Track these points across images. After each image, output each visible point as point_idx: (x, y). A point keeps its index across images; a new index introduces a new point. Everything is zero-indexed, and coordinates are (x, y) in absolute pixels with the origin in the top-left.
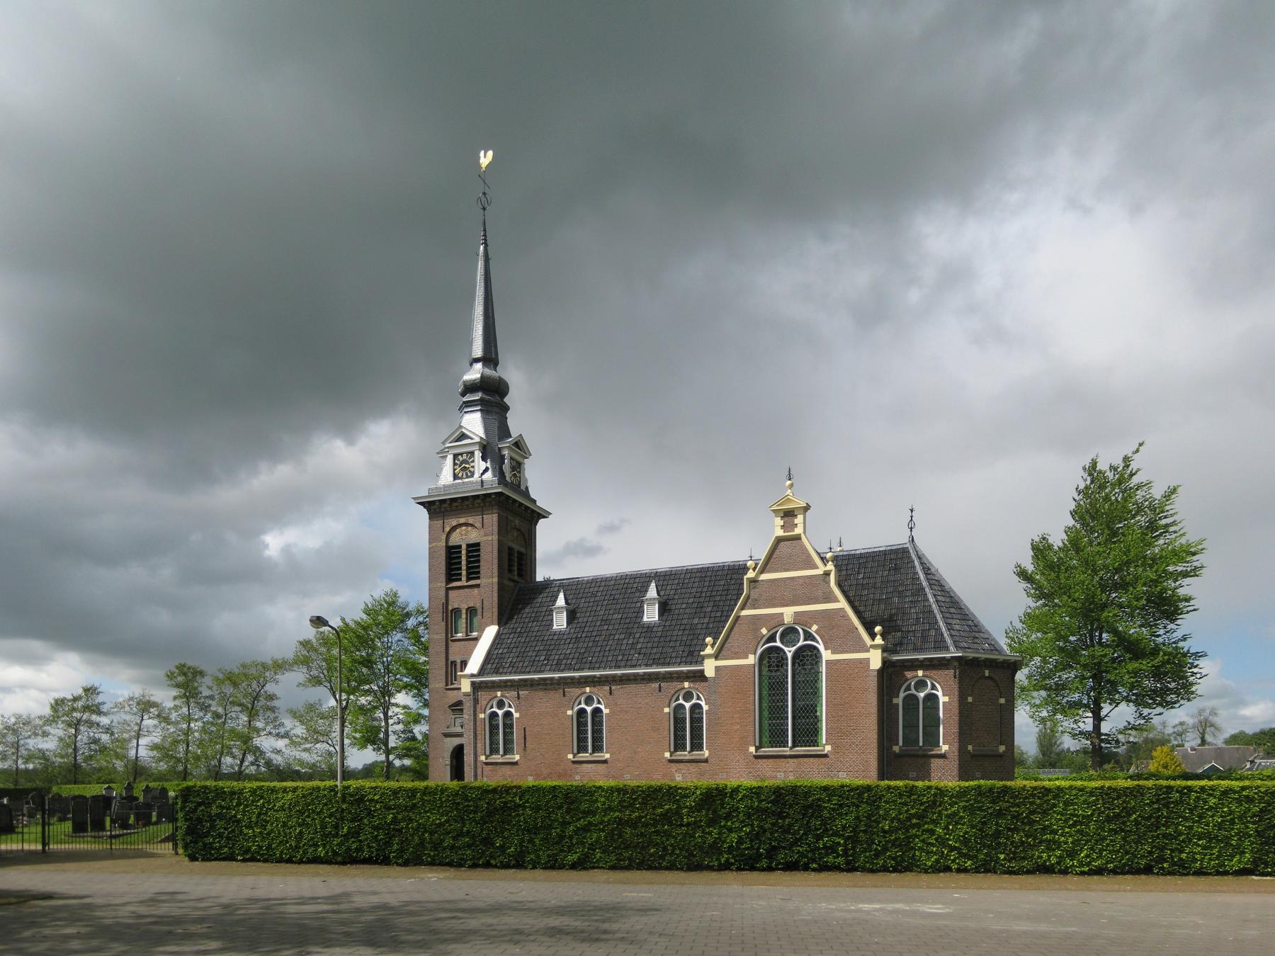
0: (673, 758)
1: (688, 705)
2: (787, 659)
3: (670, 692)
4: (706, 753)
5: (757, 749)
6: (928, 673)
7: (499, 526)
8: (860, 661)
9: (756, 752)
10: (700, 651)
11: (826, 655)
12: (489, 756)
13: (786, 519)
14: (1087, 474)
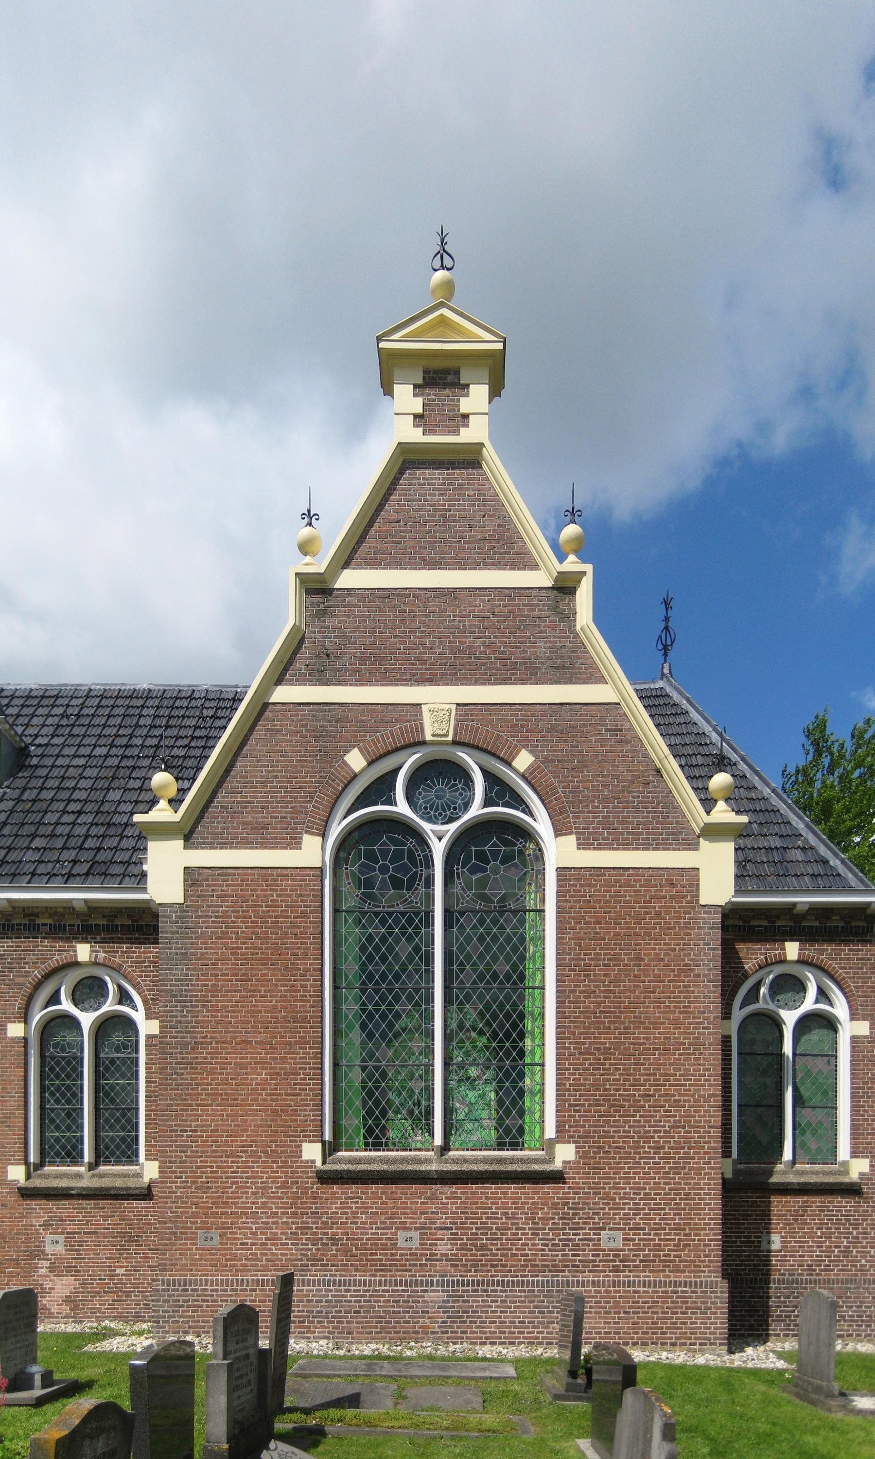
0: (37, 1183)
1: (87, 1019)
2: (429, 862)
3: (27, 975)
4: (150, 1170)
5: (330, 1149)
6: (813, 952)
8: (671, 876)
9: (324, 1163)
13: (432, 393)
14: (810, 742)
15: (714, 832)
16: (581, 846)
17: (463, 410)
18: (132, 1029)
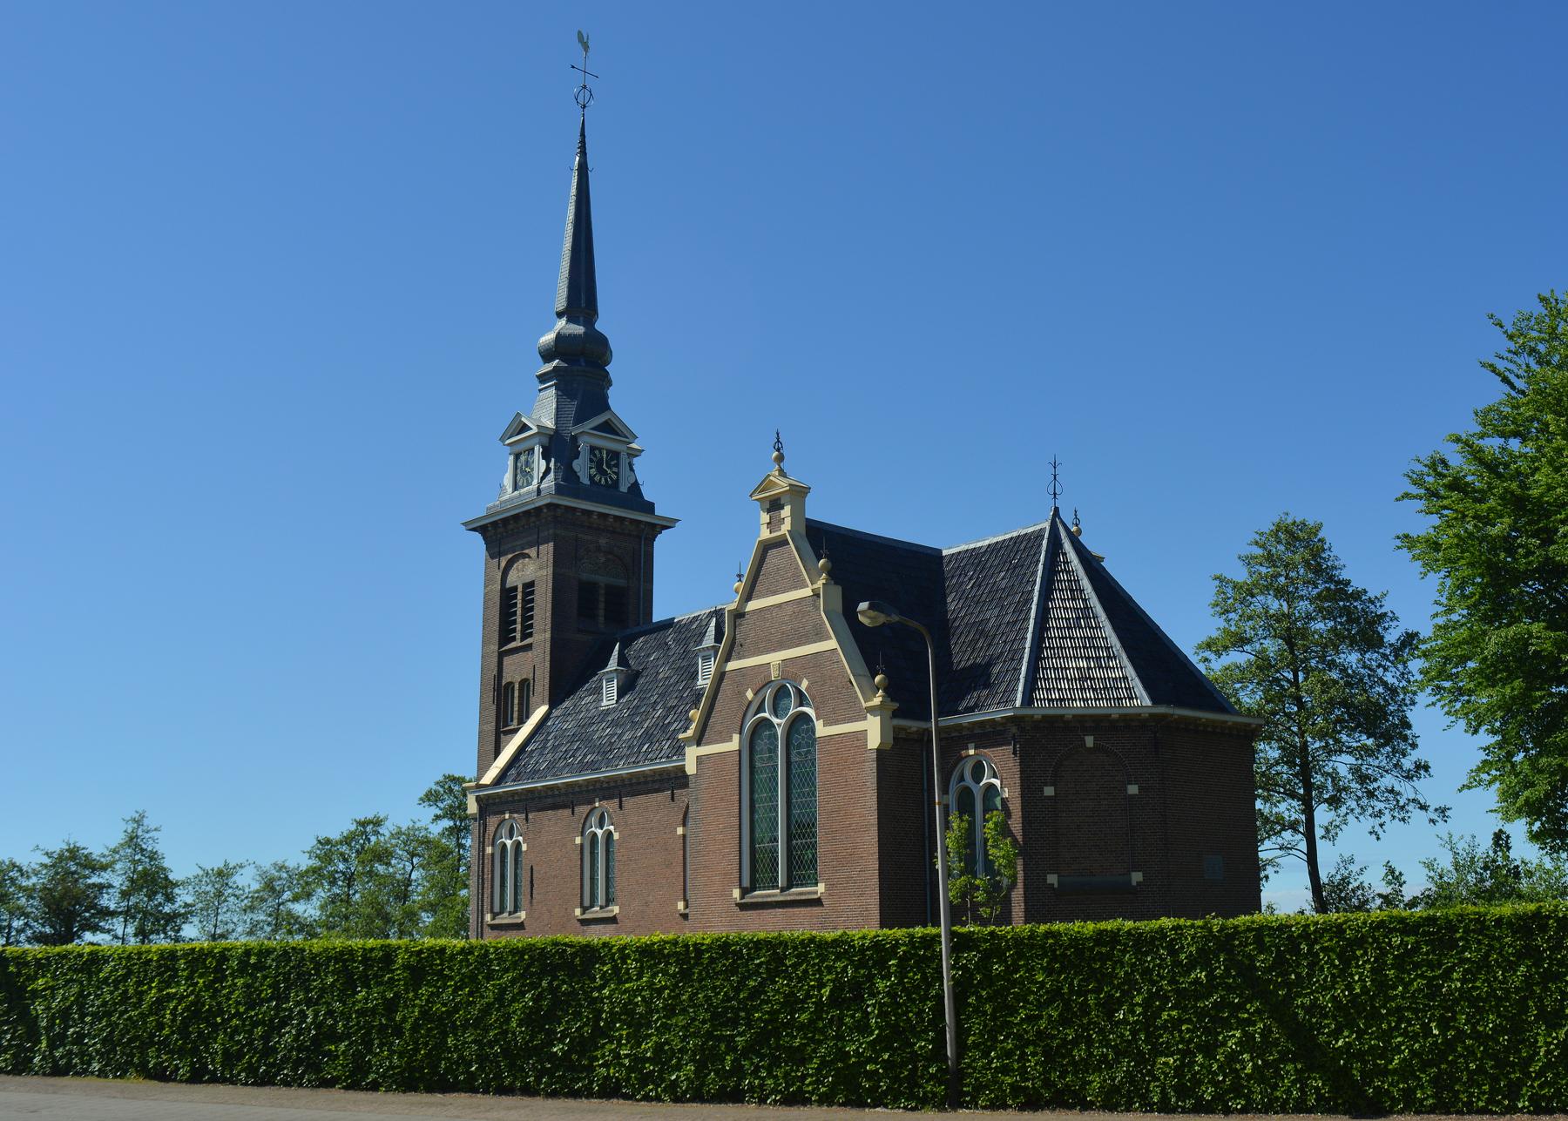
0: (587, 916)
7: (553, 593)
9: (741, 899)
10: (1054, 889)
11: (821, 730)
12: (498, 914)
15: (872, 710)
16: (569, 321)
17: (782, 517)
18: (951, 902)
